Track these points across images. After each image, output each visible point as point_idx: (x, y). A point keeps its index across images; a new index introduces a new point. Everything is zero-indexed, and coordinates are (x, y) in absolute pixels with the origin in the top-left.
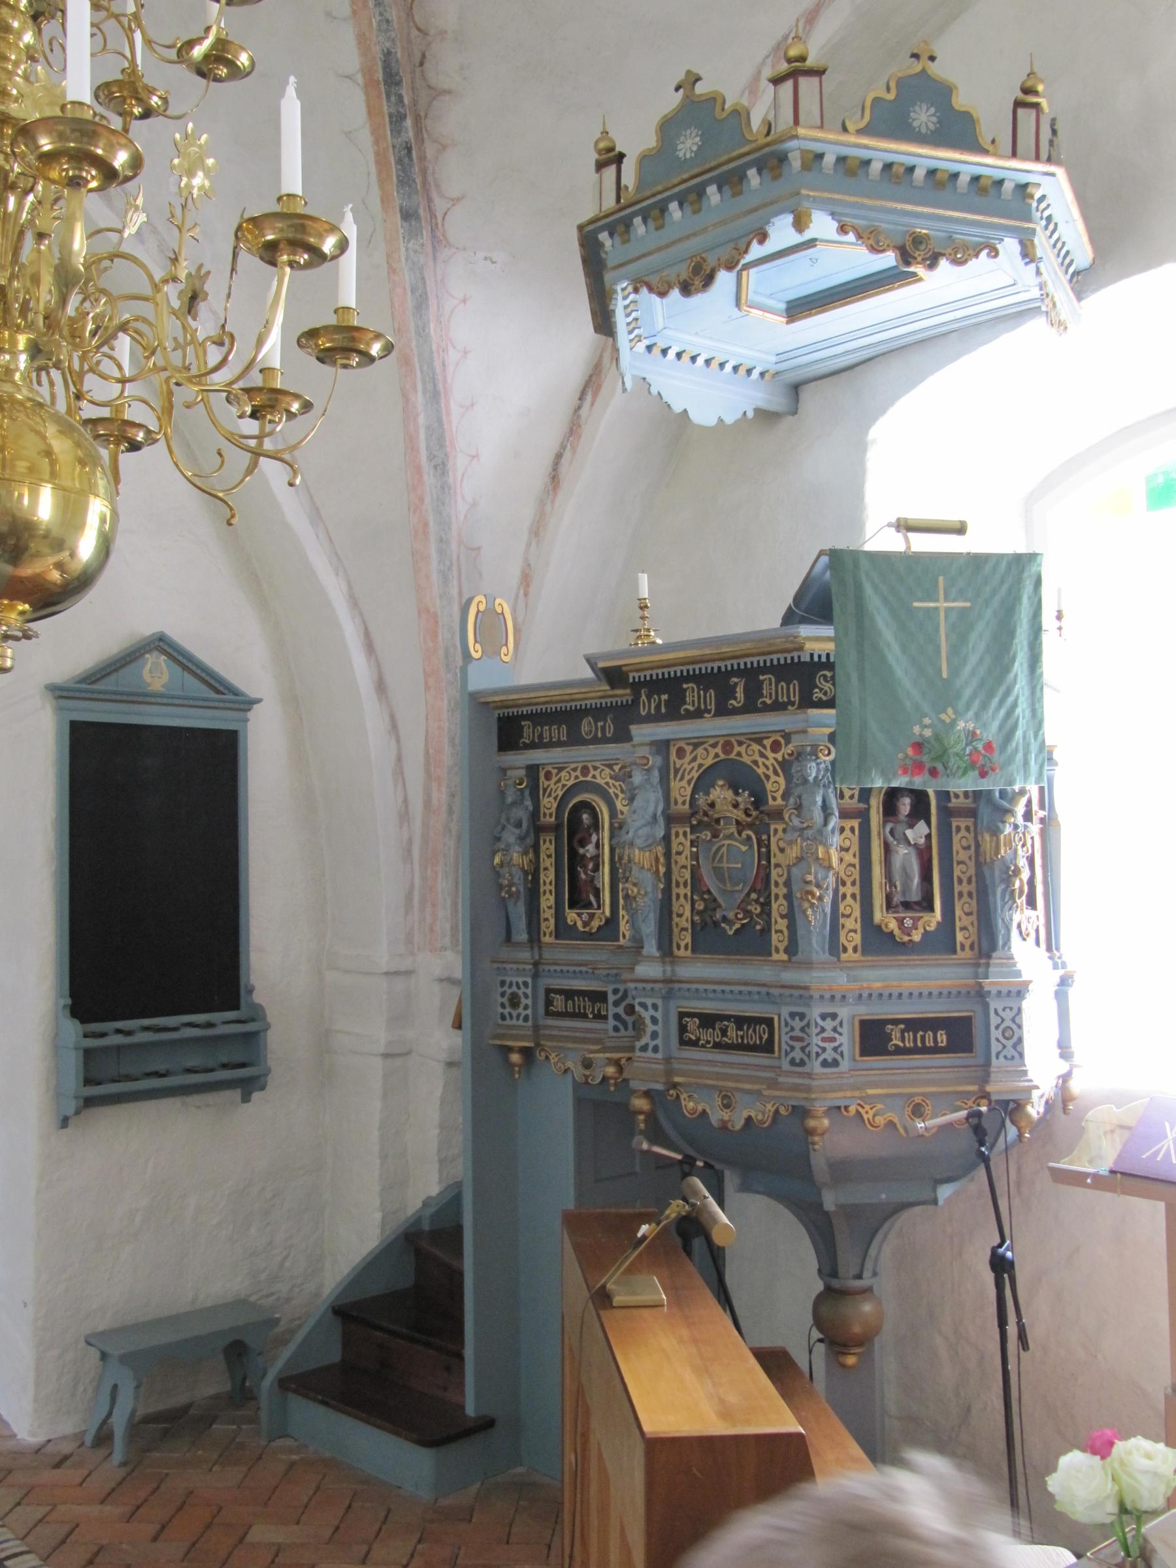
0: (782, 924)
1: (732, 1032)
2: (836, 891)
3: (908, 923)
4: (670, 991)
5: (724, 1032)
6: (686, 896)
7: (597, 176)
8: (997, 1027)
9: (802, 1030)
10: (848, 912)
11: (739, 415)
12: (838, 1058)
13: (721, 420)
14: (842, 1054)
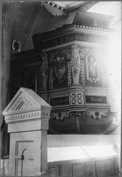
0: (70, 80)
1: (61, 101)
2: (80, 73)
3: (93, 79)
4: (49, 95)
5: (59, 101)
6: (52, 78)
7: (23, 155)
8: (111, 98)
9: (75, 97)
10: (82, 77)
11: (59, 15)
12: (82, 102)
13: (56, 15)
14: (82, 102)
